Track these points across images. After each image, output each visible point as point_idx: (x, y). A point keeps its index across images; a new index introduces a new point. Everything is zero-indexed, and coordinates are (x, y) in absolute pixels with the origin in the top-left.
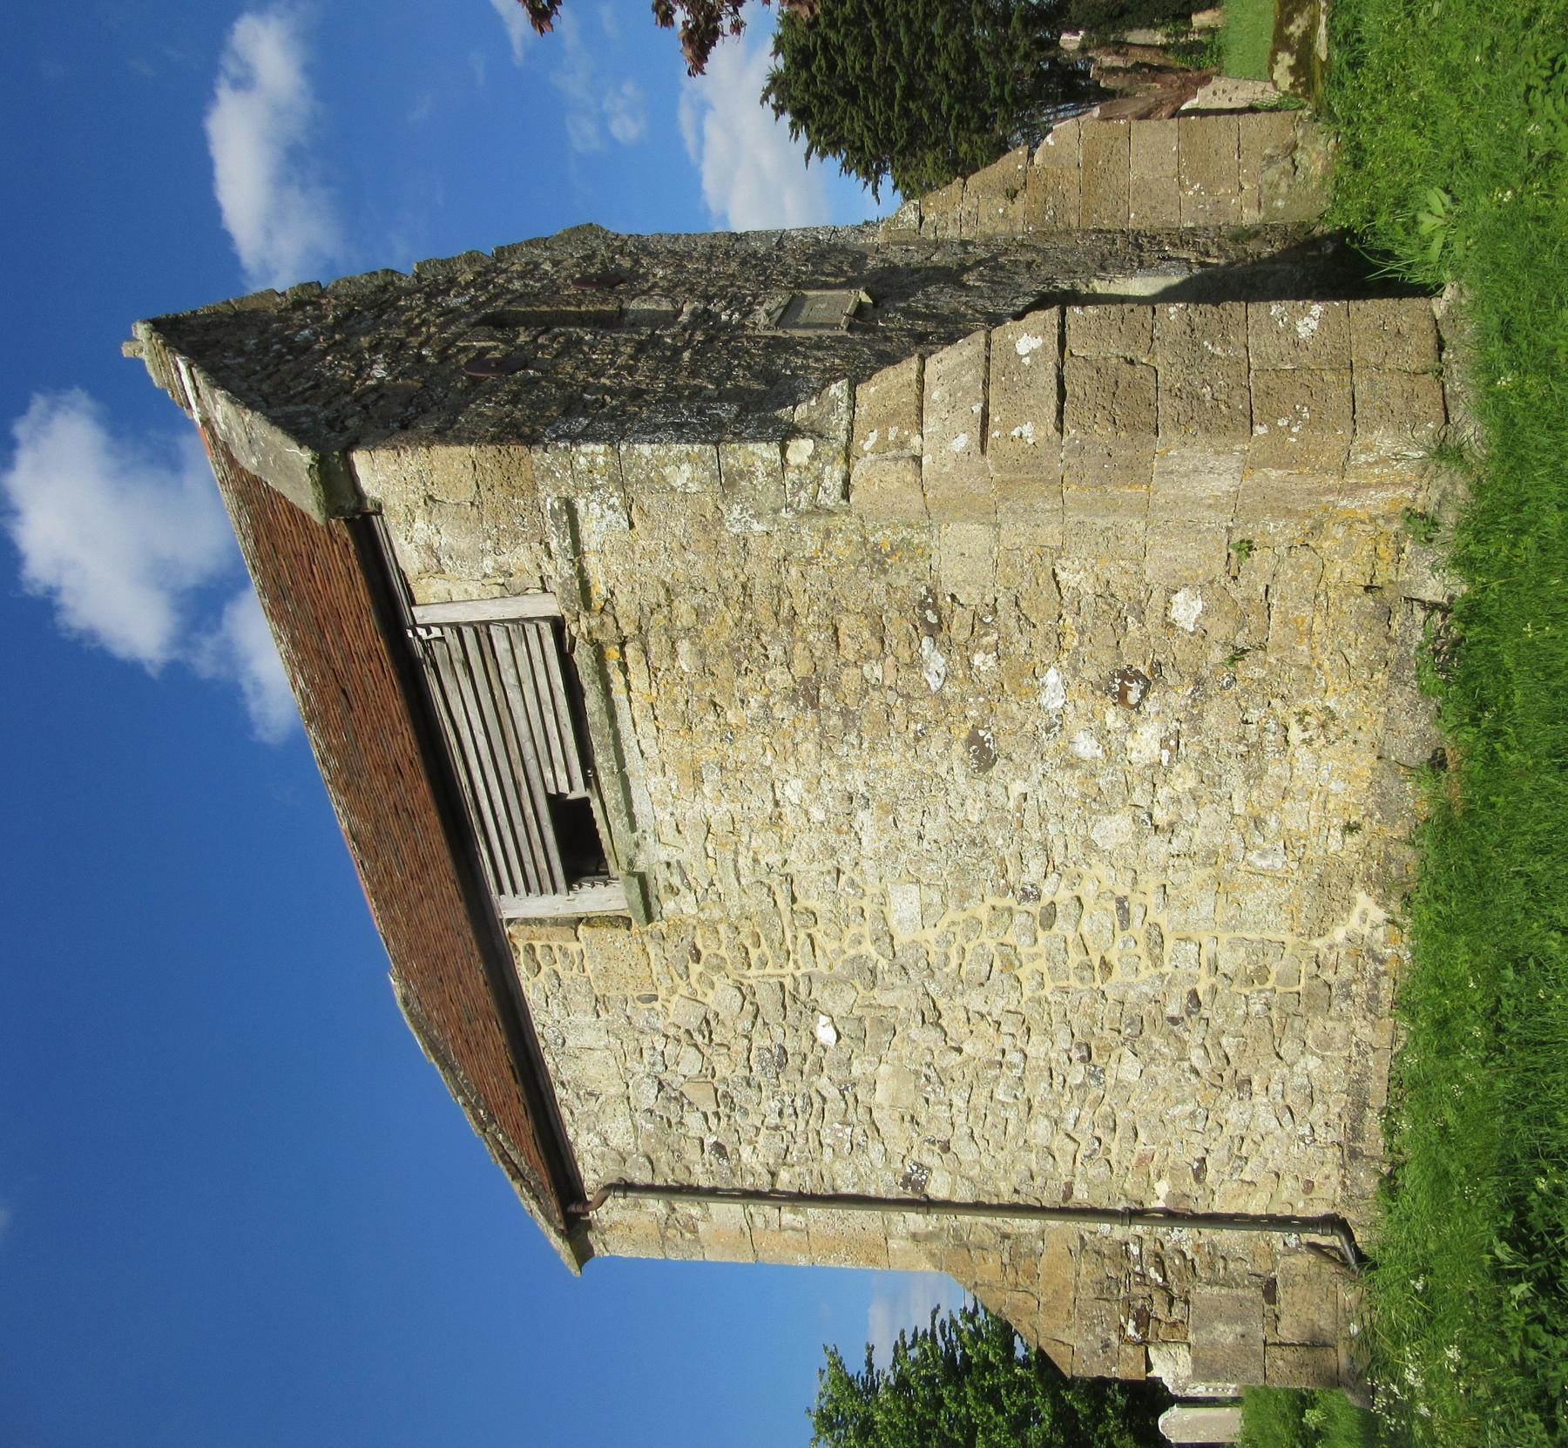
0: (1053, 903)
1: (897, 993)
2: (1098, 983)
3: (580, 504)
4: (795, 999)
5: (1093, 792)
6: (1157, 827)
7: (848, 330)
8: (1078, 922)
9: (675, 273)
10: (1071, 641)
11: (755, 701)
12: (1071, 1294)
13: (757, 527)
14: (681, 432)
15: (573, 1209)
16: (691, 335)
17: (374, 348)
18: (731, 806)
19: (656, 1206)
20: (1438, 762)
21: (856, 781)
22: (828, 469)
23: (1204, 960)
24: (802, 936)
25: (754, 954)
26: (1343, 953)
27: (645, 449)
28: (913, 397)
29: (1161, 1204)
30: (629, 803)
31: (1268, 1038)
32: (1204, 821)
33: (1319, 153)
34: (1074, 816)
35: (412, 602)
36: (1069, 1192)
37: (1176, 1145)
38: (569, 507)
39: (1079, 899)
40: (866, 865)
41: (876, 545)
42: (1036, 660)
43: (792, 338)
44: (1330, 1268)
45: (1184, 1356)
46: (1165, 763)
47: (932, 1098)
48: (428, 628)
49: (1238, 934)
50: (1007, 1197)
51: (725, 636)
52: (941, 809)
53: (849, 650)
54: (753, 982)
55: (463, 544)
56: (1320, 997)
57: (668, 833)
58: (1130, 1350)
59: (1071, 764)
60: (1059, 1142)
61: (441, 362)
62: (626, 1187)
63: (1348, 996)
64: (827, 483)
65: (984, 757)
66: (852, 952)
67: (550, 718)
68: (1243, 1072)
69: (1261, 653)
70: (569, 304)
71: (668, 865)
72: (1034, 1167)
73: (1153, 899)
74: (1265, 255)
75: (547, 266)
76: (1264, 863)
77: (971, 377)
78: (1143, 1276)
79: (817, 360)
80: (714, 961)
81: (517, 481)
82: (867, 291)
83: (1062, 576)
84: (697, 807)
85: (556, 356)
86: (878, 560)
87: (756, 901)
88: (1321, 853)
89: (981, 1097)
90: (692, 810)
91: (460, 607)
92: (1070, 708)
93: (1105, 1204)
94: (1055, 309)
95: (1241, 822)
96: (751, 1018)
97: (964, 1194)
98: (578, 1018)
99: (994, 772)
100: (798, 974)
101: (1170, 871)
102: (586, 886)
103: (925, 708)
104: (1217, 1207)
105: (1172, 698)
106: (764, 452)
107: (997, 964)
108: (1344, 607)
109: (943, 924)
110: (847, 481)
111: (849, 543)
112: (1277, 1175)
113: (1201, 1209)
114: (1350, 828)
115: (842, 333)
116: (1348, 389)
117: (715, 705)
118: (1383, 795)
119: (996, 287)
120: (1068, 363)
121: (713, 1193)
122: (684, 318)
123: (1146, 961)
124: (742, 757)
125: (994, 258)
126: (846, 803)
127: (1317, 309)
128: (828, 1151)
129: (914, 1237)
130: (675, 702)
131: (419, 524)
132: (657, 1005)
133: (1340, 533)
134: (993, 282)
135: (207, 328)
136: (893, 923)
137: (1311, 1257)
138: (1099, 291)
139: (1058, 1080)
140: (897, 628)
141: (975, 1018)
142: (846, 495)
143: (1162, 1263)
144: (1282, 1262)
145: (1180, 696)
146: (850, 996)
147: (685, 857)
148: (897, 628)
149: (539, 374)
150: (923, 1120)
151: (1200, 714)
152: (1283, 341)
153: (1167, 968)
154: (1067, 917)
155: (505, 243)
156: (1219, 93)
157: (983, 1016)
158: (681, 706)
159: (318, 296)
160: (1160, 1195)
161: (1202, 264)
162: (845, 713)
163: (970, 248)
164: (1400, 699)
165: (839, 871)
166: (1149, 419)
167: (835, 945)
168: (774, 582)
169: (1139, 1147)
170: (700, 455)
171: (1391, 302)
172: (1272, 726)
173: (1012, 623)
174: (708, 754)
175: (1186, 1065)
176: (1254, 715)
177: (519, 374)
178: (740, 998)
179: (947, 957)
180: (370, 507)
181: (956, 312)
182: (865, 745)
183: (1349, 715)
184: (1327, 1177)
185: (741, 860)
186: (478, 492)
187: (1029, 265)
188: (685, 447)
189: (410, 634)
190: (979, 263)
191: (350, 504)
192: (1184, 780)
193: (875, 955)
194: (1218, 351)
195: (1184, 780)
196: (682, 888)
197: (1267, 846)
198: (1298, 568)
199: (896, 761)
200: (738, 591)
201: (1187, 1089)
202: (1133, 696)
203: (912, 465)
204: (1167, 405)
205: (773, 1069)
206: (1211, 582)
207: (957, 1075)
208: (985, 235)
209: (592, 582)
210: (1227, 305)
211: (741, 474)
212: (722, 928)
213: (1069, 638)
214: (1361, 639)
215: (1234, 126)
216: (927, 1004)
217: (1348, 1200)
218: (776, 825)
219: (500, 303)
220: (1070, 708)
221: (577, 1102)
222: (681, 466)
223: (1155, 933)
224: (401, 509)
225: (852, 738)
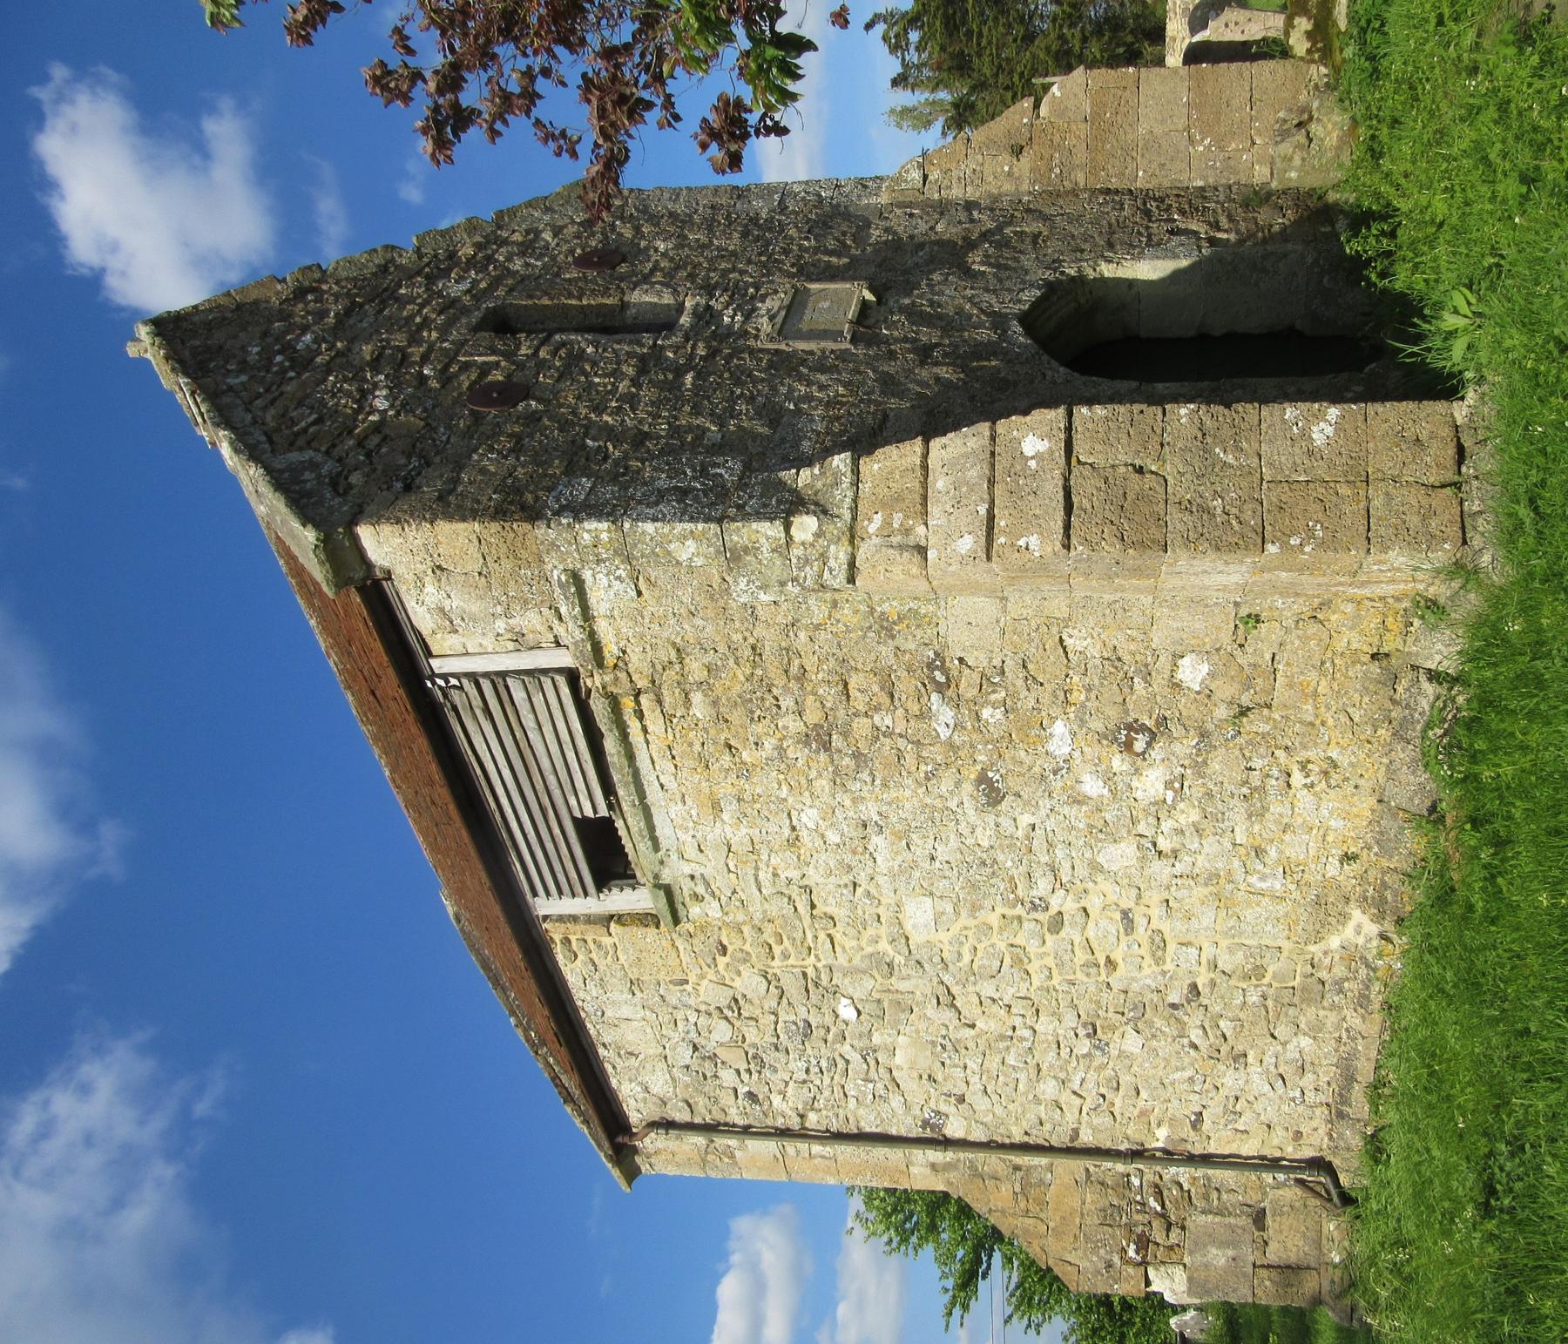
0: (1060, 913)
1: (914, 981)
2: (1103, 977)
3: (587, 575)
4: (817, 985)
5: (1100, 824)
6: (1160, 853)
7: (851, 341)
8: (1084, 928)
9: (676, 247)
10: (1078, 696)
11: (769, 744)
12: (1077, 1221)
13: (764, 598)
14: (685, 515)
15: (620, 1139)
16: (693, 348)
17: (375, 365)
18: (751, 831)
19: (699, 1140)
20: (1434, 814)
21: (870, 811)
22: (833, 547)
23: (1204, 960)
24: (822, 936)
25: (777, 950)
26: (1337, 958)
27: (649, 527)
28: (918, 485)
29: (1160, 1145)
30: (651, 828)
31: (1264, 1023)
32: (1207, 849)
33: (1335, 124)
34: (1081, 842)
35: (429, 654)
36: (1076, 1133)
37: (1176, 1103)
38: (577, 579)
39: (1085, 910)
40: (881, 880)
41: (883, 614)
42: (1044, 714)
43: (795, 351)
44: (1314, 1202)
45: (1179, 1274)
46: (1169, 801)
47: (947, 1062)
48: (445, 677)
49: (1237, 940)
50: (1018, 1138)
51: (737, 689)
52: (952, 836)
53: (859, 701)
54: (778, 972)
55: (475, 607)
56: (1315, 989)
57: (691, 852)
58: (1131, 1270)
59: (1079, 800)
60: (1065, 1097)
61: (443, 387)
62: (668, 1125)
63: (1341, 991)
64: (832, 563)
65: (992, 794)
66: (869, 950)
67: (570, 755)
68: (1239, 1048)
69: (1266, 711)
70: (570, 296)
71: (692, 877)
72: (1043, 1116)
73: (1157, 911)
74: (1276, 228)
75: (547, 236)
76: (1264, 885)
77: (975, 473)
78: (1144, 1204)
79: (822, 388)
80: (740, 955)
81: (524, 554)
82: (872, 289)
83: (1068, 642)
84: (718, 831)
85: (558, 380)
86: (886, 628)
87: (777, 907)
88: (1319, 877)
89: (993, 1063)
90: (713, 834)
91: (477, 659)
92: (1077, 754)
93: (1108, 1145)
94: (1061, 411)
95: (1242, 851)
96: (776, 999)
97: (978, 1135)
98: (615, 996)
99: (1004, 806)
100: (819, 965)
101: (1173, 889)
102: (615, 891)
103: (936, 753)
104: (1213, 1148)
105: (1177, 747)
106: (769, 531)
107: (1007, 961)
108: (1350, 674)
109: (955, 929)
110: (852, 565)
111: (856, 612)
112: (1269, 1127)
113: (1198, 1150)
114: (1348, 858)
115: (846, 345)
116: (1363, 504)
117: (730, 747)
118: (1381, 833)
119: (1004, 274)
120: (1075, 471)
121: (746, 1131)
122: (685, 320)
123: (1148, 960)
124: (759, 790)
125: (1000, 228)
126: (860, 830)
127: (1333, 412)
128: (852, 1103)
129: (933, 1166)
130: (691, 745)
131: (429, 589)
132: (689, 988)
133: (1349, 608)
134: (998, 266)
135: (209, 326)
136: (908, 927)
137: (1299, 1191)
138: (1106, 275)
139: (1065, 1052)
140: (906, 685)
141: (987, 1002)
142: (851, 580)
143: (1161, 1193)
144: (1272, 1194)
145: (1185, 746)
146: (869, 984)
147: (708, 872)
148: (906, 685)
149: (541, 407)
150: (939, 1078)
151: (1205, 762)
152: (1297, 450)
153: (1169, 966)
154: (1073, 924)
155: (504, 208)
156: (1232, 25)
157: (994, 1000)
158: (697, 748)
159: (319, 281)
160: (1160, 1138)
161: (1212, 241)
162: (857, 755)
163: (975, 213)
164: (1403, 754)
165: (855, 884)
166: (1159, 536)
167: (854, 943)
168: (783, 644)
169: (1141, 1104)
170: (703, 532)
171: (1408, 406)
172: (1275, 772)
173: (1020, 683)
174: (725, 789)
175: (1186, 1041)
176: (1257, 763)
177: (521, 406)
178: (765, 983)
179: (960, 954)
180: (379, 574)
181: (959, 311)
182: (878, 782)
183: (1351, 764)
184: (1315, 1129)
185: (761, 875)
186: (485, 563)
187: (1035, 237)
188: (689, 526)
189: (429, 684)
190: (985, 236)
191: (359, 574)
192: (1188, 815)
193: (891, 953)
194: (1230, 459)
195: (1188, 815)
196: (707, 896)
197: (1267, 871)
198: (1305, 639)
199: (909, 797)
200: (748, 652)
201: (1187, 1060)
202: (1139, 746)
203: (917, 558)
204: (1175, 517)
205: (799, 1038)
206: (1218, 650)
207: (971, 1045)
208: (990, 195)
209: (604, 642)
210: (1239, 407)
211: (746, 550)
212: (746, 929)
213: (1075, 694)
214: (1366, 699)
215: (1246, 74)
216: (941, 990)
217: (1335, 1149)
218: (793, 845)
219: (501, 292)
220: (1077, 754)
221: (618, 1060)
222: (687, 543)
223: (1157, 939)
224: (411, 577)
225: (865, 776)
